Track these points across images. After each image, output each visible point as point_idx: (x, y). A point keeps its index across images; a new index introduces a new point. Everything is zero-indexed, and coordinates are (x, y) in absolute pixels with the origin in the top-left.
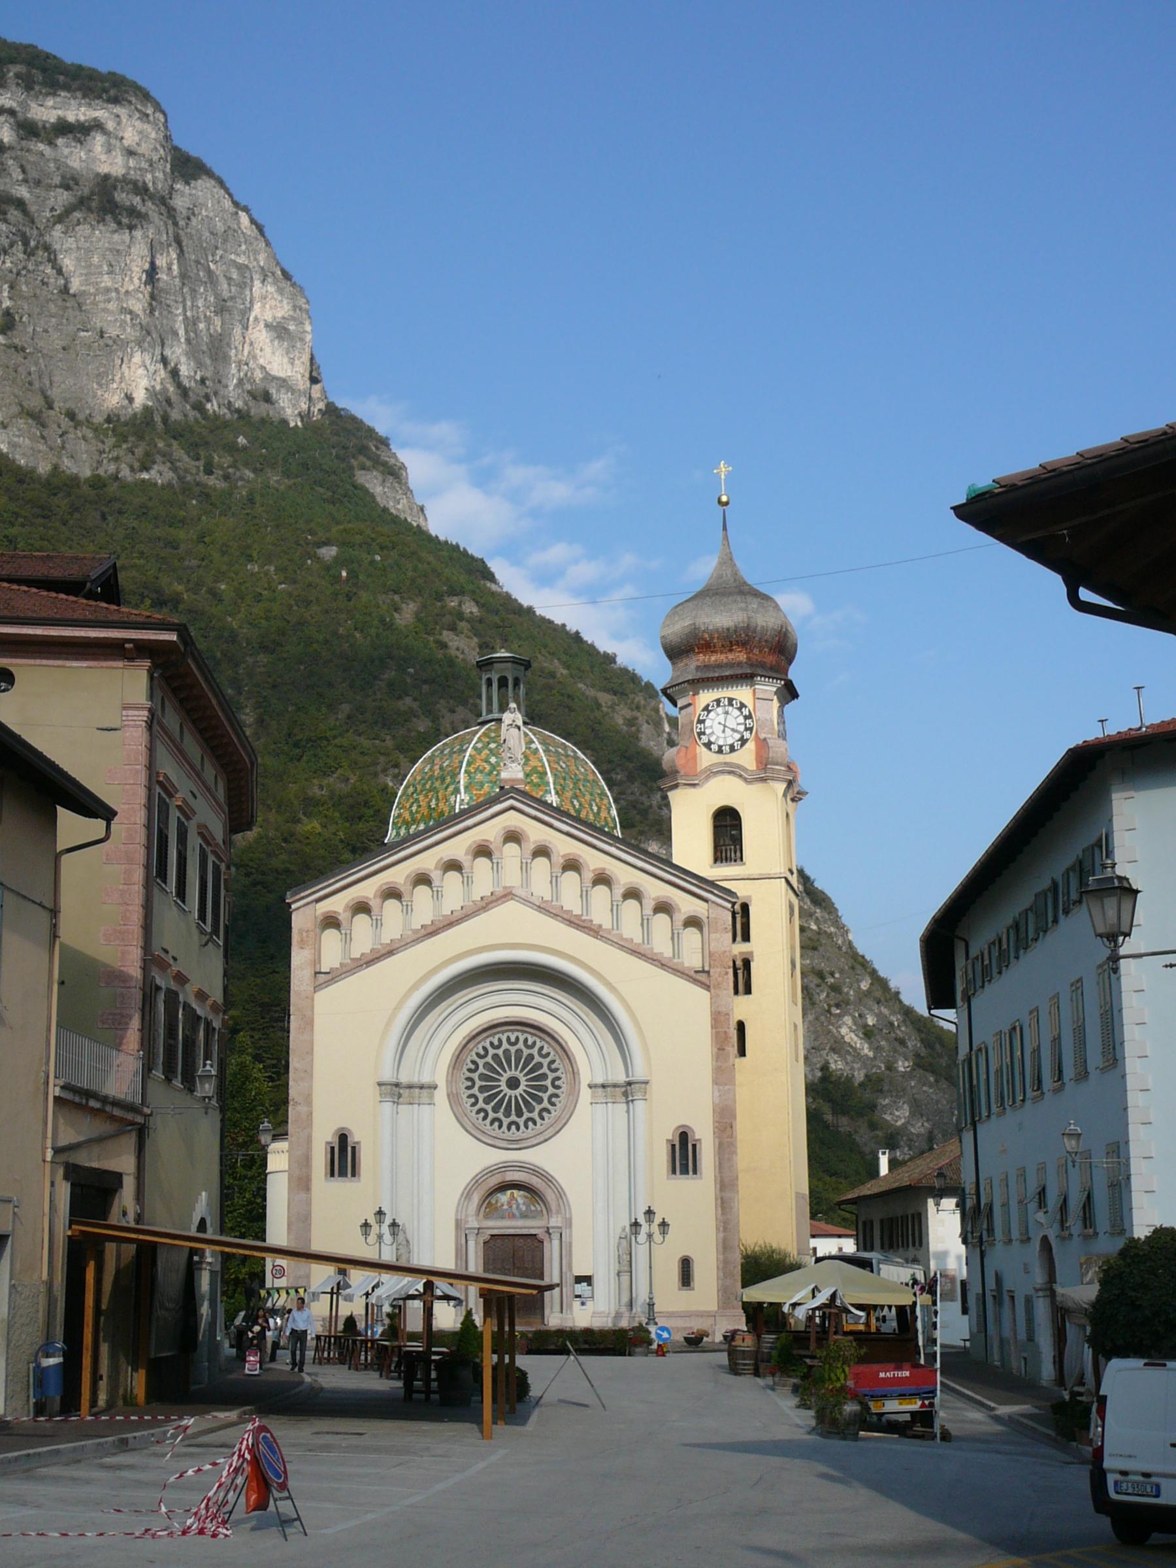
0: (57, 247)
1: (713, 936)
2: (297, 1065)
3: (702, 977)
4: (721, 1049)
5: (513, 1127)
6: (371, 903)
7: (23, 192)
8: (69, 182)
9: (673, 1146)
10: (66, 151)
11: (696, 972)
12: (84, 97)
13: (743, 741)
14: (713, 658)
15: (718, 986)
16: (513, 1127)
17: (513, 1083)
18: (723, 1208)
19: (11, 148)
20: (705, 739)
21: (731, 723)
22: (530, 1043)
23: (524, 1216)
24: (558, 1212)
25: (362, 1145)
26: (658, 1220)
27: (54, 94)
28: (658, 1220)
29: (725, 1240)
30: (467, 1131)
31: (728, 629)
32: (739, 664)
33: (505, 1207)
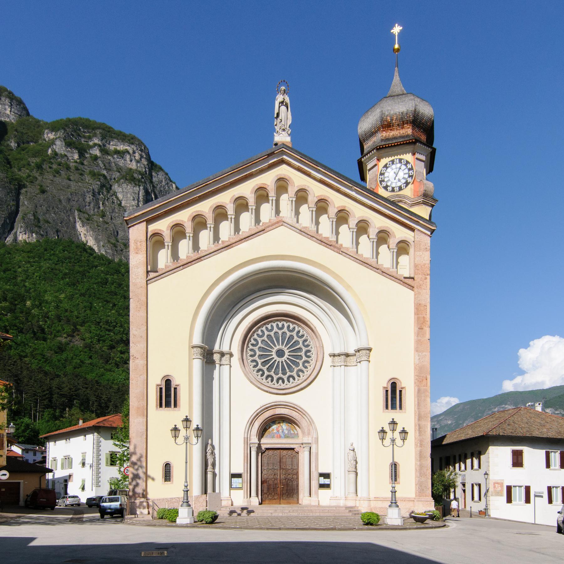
1: (418, 253)
3: (409, 281)
4: (421, 328)
5: (280, 381)
7: (105, 172)
8: (119, 170)
9: (387, 391)
10: (118, 160)
11: (405, 278)
13: (407, 184)
14: (391, 134)
15: (420, 287)
16: (280, 381)
17: (280, 353)
18: (420, 432)
20: (384, 184)
22: (291, 328)
23: (286, 437)
24: (309, 434)
25: (181, 386)
26: (399, 429)
27: (113, 141)
28: (399, 429)
29: (421, 452)
30: (251, 382)
31: (402, 113)
33: (275, 431)
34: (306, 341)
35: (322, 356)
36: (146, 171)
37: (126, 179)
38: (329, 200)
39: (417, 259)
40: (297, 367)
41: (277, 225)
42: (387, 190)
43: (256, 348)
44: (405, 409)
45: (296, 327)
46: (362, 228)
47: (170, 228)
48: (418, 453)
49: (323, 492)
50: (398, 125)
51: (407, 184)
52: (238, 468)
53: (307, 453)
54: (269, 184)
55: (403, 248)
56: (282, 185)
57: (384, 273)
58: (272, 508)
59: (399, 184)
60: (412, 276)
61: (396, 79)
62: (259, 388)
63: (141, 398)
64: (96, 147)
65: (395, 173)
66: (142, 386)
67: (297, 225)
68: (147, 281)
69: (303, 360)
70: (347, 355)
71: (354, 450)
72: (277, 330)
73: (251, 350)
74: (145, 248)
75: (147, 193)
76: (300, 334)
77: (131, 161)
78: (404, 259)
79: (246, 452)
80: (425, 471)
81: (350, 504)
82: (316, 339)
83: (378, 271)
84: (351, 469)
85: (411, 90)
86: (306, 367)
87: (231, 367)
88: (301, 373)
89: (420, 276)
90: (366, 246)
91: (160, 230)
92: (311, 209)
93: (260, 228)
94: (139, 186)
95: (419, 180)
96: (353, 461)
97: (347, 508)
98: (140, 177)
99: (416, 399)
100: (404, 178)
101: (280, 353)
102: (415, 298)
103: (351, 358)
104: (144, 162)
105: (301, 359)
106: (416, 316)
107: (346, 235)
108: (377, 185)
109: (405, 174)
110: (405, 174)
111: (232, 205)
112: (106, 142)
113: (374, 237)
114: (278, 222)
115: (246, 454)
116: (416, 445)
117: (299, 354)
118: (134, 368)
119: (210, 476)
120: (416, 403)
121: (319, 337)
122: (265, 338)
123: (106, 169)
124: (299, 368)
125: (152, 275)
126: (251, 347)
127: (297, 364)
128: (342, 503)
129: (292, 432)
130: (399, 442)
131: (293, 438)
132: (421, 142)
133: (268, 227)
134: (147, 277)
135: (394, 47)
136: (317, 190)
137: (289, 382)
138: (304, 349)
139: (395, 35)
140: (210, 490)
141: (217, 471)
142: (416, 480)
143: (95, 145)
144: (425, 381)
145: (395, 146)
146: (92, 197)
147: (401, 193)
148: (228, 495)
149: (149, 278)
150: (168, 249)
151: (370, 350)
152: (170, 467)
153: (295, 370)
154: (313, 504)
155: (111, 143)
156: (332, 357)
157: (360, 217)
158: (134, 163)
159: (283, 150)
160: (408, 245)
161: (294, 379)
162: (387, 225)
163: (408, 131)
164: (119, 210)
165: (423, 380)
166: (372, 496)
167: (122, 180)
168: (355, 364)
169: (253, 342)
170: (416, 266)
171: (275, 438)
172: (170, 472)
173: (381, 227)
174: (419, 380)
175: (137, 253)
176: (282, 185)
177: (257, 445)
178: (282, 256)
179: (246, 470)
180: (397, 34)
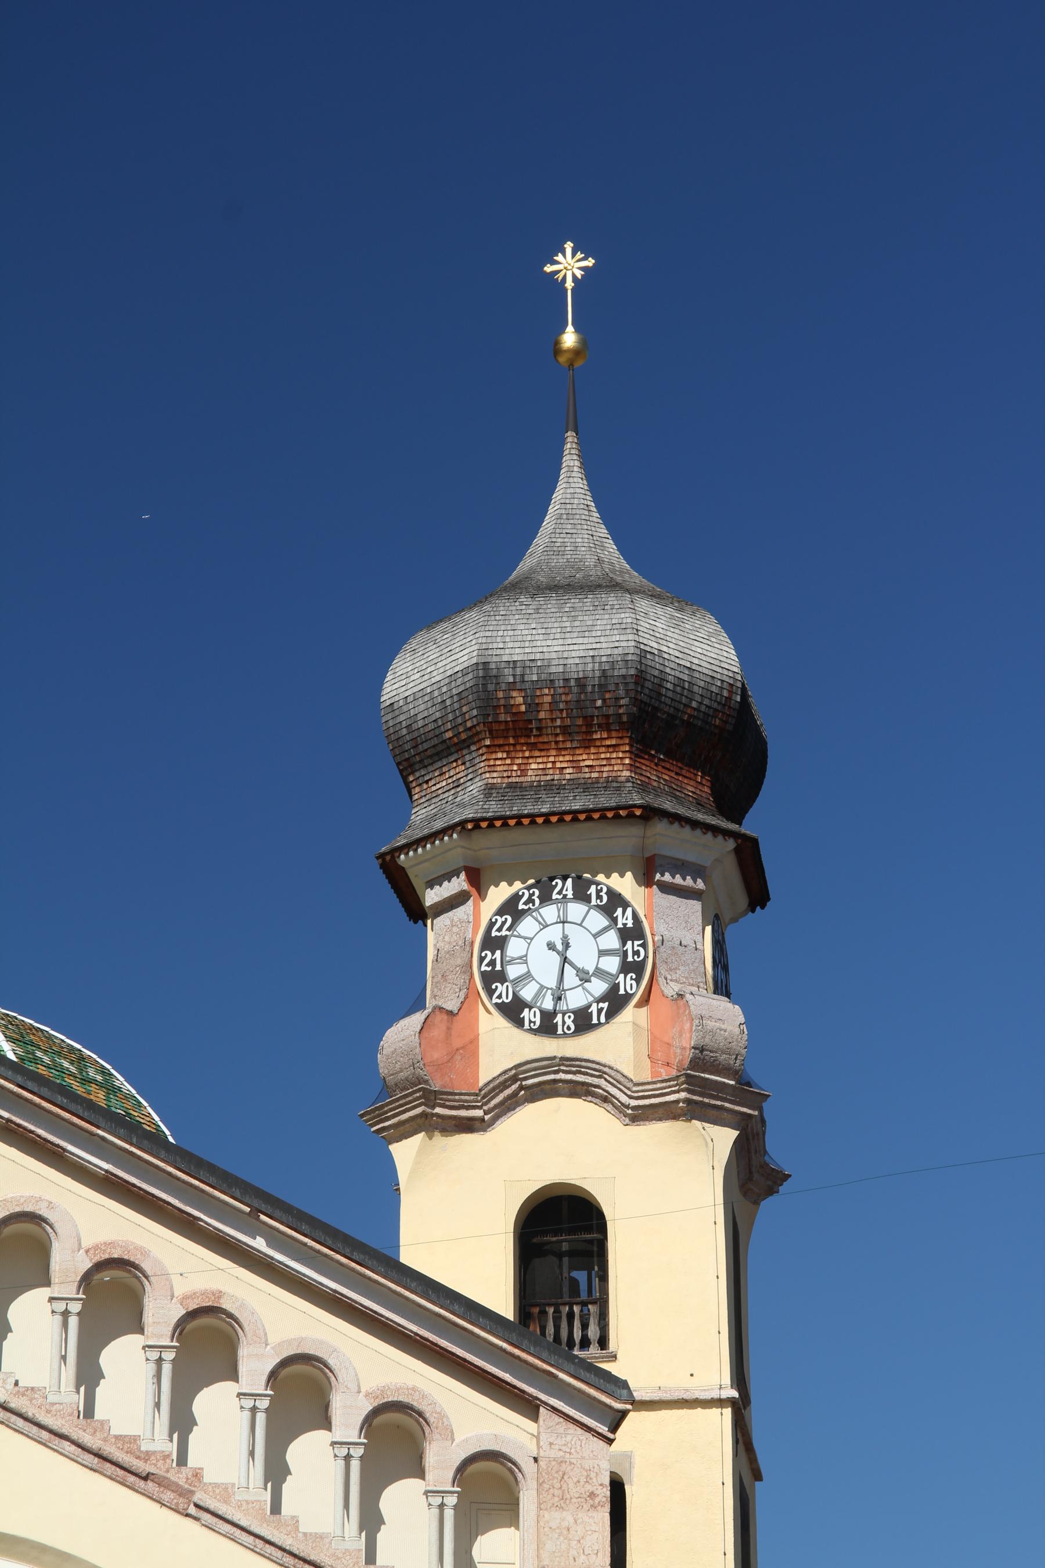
1: (554, 1518)
13: (615, 1001)
21: (584, 954)
31: (581, 683)
32: (611, 784)
39: (549, 1546)
42: (519, 1023)
46: (300, 1392)
50: (565, 730)
61: (571, 487)
65: (551, 946)
92: (60, 1306)
100: (599, 973)
108: (470, 997)
109: (602, 953)
110: (602, 953)
135: (557, 343)
157: (289, 1342)
162: (412, 1380)
173: (383, 1391)
180: (569, 284)
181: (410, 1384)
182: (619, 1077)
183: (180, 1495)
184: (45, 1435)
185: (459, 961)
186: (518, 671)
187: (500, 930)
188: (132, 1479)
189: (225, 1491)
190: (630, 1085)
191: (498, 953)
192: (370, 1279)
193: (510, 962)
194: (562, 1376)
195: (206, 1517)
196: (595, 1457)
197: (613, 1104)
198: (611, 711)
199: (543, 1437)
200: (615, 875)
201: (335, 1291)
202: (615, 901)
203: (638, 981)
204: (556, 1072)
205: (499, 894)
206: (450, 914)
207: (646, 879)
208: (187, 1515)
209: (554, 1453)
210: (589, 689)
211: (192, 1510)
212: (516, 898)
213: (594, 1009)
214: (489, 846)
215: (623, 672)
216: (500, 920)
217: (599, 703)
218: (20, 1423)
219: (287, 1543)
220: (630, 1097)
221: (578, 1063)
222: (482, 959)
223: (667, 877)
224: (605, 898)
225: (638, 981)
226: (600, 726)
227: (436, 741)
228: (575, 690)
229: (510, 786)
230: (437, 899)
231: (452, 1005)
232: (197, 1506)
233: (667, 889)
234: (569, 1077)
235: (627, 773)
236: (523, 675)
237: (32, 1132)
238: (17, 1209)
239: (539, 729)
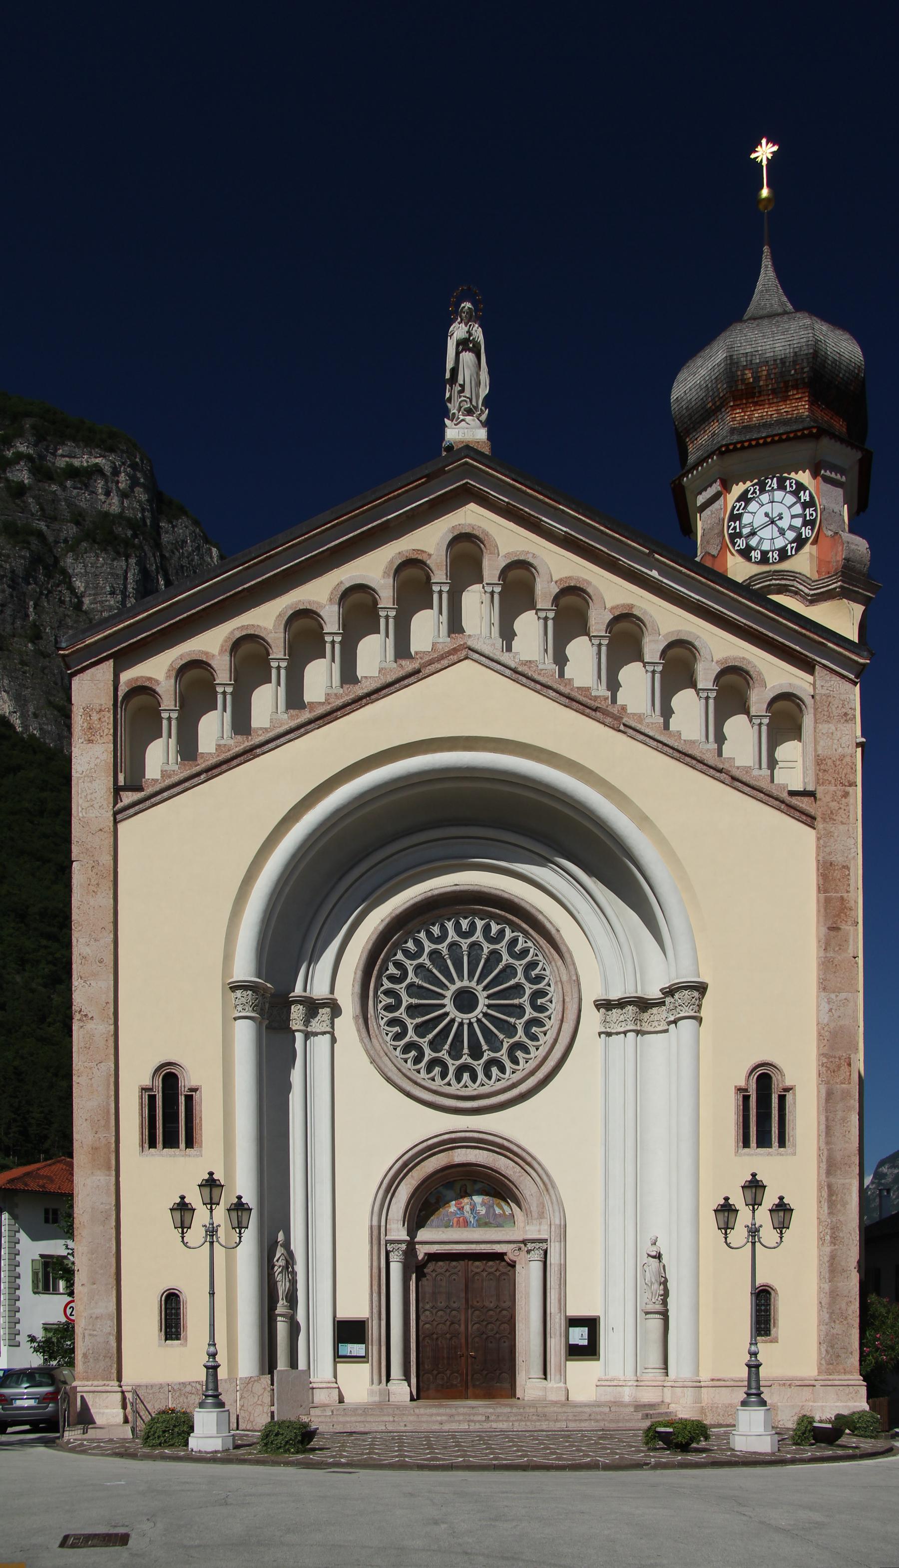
0: (70, 571)
1: (824, 728)
2: (86, 951)
3: (804, 803)
4: (834, 929)
5: (466, 1076)
6: (214, 663)
7: (42, 526)
8: (78, 518)
10: (75, 491)
11: (792, 793)
12: (86, 446)
13: (800, 542)
15: (830, 817)
17: (465, 1000)
18: (832, 1204)
19: (30, 488)
20: (741, 543)
23: (483, 1223)
24: (541, 1215)
26: (770, 1199)
27: (63, 444)
28: (770, 1199)
29: (833, 1257)
30: (389, 1080)
31: (783, 361)
34: (533, 965)
35: (576, 1006)
36: (144, 519)
37: (94, 541)
38: (589, 590)
39: (822, 743)
40: (511, 1037)
41: (454, 658)
42: (749, 559)
43: (401, 988)
44: (794, 1145)
45: (508, 931)
47: (174, 673)
48: (826, 1259)
49: (578, 1368)
50: (774, 391)
51: (800, 542)
52: (356, 1305)
53: (535, 1268)
54: (431, 551)
55: (785, 717)
56: (466, 552)
57: (736, 781)
58: (442, 1411)
59: (780, 543)
60: (810, 788)
61: (767, 276)
62: (408, 1095)
63: (103, 1122)
64: (22, 463)
66: (107, 1090)
67: (506, 658)
68: (115, 814)
69: (526, 1017)
70: (643, 1005)
71: (659, 1257)
72: (457, 938)
73: (387, 993)
74: (111, 726)
75: (144, 573)
76: (518, 949)
77: (108, 493)
78: (789, 751)
79: (375, 1264)
80: (844, 1306)
81: (649, 1396)
82: (560, 962)
83: (723, 776)
84: (650, 1307)
85: (804, 297)
86: (534, 1038)
87: (334, 1040)
88: (520, 1054)
89: (832, 788)
90: (689, 712)
91: (150, 679)
93: (409, 666)
94: (127, 557)
95: (830, 533)
96: (655, 1286)
97: (638, 1407)
98: (130, 533)
99: (823, 1118)
100: (791, 528)
101: (465, 1000)
102: (818, 847)
103: (655, 1010)
104: (141, 495)
105: (521, 1016)
106: (822, 896)
107: (636, 685)
108: (723, 547)
109: (793, 517)
110: (793, 517)
111: (336, 608)
112: (47, 450)
113: (710, 685)
114: (455, 651)
115: (375, 1271)
116: (821, 1239)
117: (516, 1001)
118: (82, 1044)
119: (282, 1328)
120: (823, 1127)
121: (566, 955)
122: (424, 959)
123: (44, 516)
124: (516, 1039)
125: (128, 798)
126: (387, 984)
127: (511, 1030)
128: (627, 1395)
129: (498, 1211)
130: (768, 1234)
131: (499, 1225)
132: (833, 436)
133: (431, 662)
134: (114, 807)
136: (557, 566)
137: (490, 1078)
138: (529, 989)
139: (768, 186)
140: (282, 1363)
141: (301, 1317)
142: (819, 1330)
143: (19, 456)
144: (845, 1068)
145: (765, 444)
146: (8, 591)
147: (785, 566)
148: (329, 1376)
149: (120, 805)
150: (225, 710)
151: (701, 988)
152: (178, 1302)
153: (506, 1046)
154: (552, 1397)
155: (60, 452)
156: (602, 1010)
157: (672, 633)
158: (115, 500)
159: (466, 463)
160: (798, 706)
161: (502, 1069)
162: (742, 654)
163: (799, 407)
164: (76, 622)
165: (839, 1067)
166: (705, 1375)
167: (84, 544)
168: (663, 1026)
169: (392, 970)
170: (819, 761)
171: (455, 1230)
172: (178, 1314)
173: (726, 659)
174: (832, 1063)
175: (90, 741)
176: (466, 552)
177: (404, 1246)
178: (468, 738)
179: (375, 1311)
180: (764, 163)
181: (741, 656)
182: (804, 578)
183: (615, 719)
184: (538, 687)
185: (716, 531)
186: (749, 358)
187: (738, 510)
188: (588, 711)
189: (640, 717)
190: (810, 582)
191: (738, 522)
192: (718, 591)
193: (744, 527)
194: (830, 645)
195: (630, 731)
196: (847, 693)
197: (801, 595)
198: (799, 377)
199: (818, 682)
200: (800, 472)
201: (698, 600)
202: (800, 487)
203: (812, 530)
204: (770, 580)
205: (738, 489)
206: (710, 508)
207: (815, 474)
208: (620, 731)
209: (824, 692)
210: (787, 364)
211: (622, 728)
212: (746, 492)
213: (789, 547)
214: (734, 461)
215: (806, 352)
216: (738, 505)
217: (793, 372)
218: (524, 680)
219: (676, 745)
220: (810, 589)
221: (508, 1154)
222: (729, 527)
223: (828, 473)
224: (794, 487)
225: (812, 530)
226: (792, 386)
227: (702, 412)
228: (780, 366)
229: (744, 427)
230: (703, 501)
231: (715, 553)
232: (625, 725)
233: (827, 480)
234: (778, 582)
235: (807, 413)
236: (751, 361)
237: (522, 510)
238: (516, 558)
239: (760, 392)
